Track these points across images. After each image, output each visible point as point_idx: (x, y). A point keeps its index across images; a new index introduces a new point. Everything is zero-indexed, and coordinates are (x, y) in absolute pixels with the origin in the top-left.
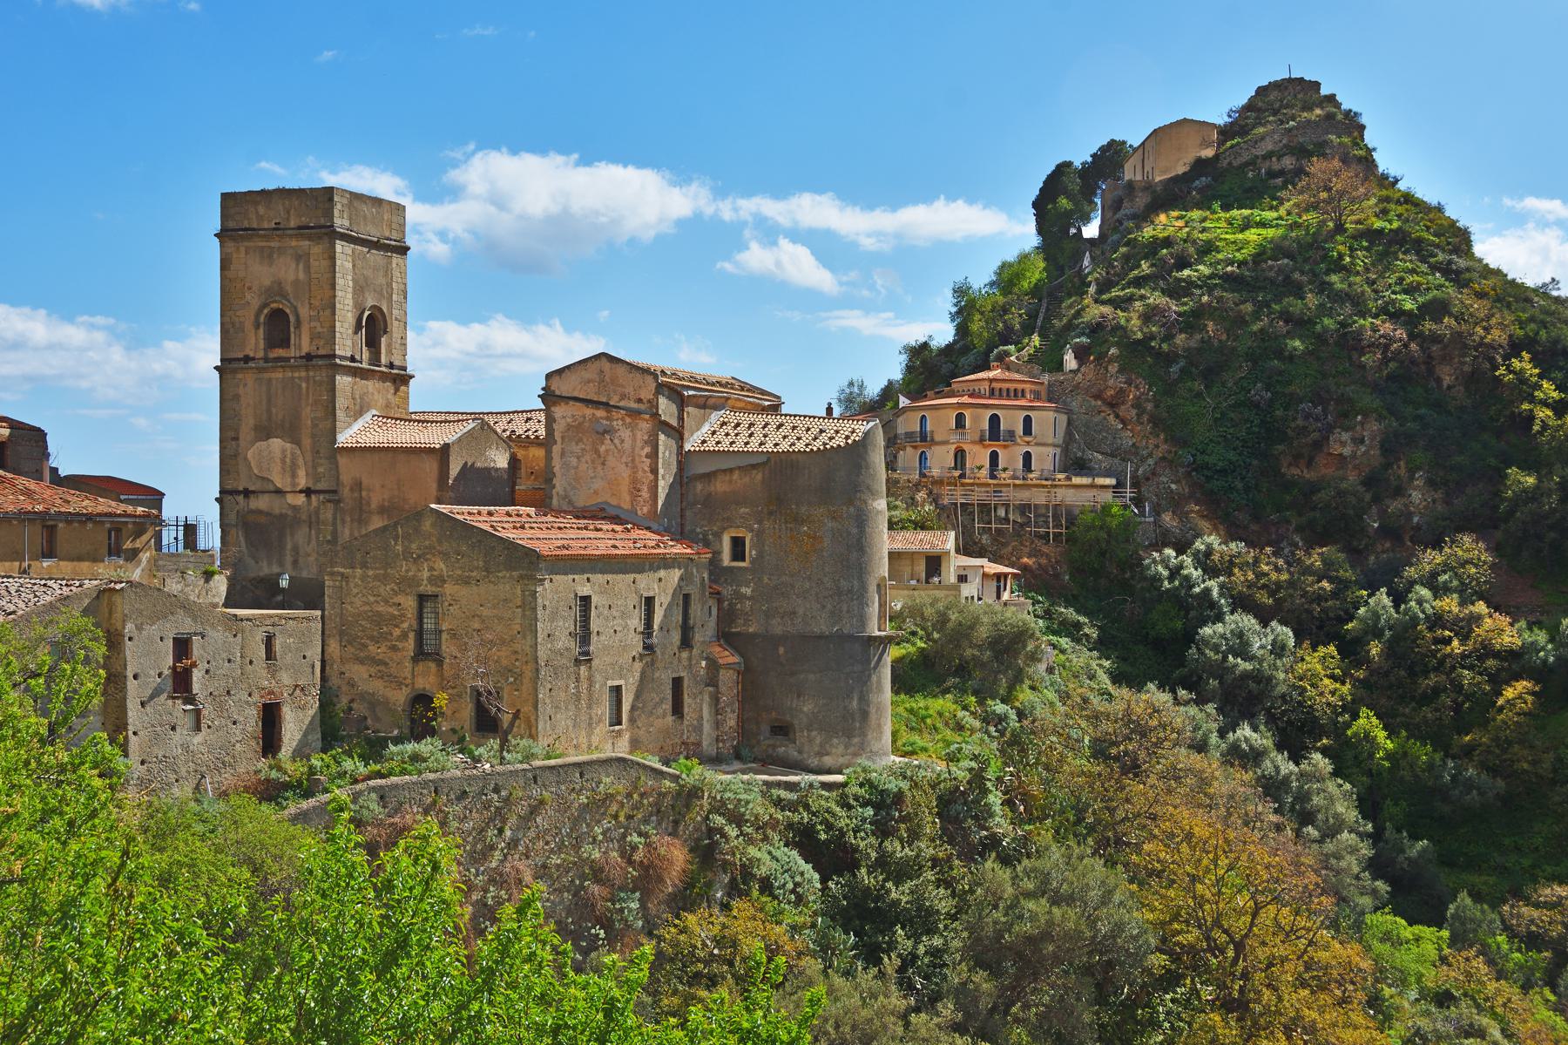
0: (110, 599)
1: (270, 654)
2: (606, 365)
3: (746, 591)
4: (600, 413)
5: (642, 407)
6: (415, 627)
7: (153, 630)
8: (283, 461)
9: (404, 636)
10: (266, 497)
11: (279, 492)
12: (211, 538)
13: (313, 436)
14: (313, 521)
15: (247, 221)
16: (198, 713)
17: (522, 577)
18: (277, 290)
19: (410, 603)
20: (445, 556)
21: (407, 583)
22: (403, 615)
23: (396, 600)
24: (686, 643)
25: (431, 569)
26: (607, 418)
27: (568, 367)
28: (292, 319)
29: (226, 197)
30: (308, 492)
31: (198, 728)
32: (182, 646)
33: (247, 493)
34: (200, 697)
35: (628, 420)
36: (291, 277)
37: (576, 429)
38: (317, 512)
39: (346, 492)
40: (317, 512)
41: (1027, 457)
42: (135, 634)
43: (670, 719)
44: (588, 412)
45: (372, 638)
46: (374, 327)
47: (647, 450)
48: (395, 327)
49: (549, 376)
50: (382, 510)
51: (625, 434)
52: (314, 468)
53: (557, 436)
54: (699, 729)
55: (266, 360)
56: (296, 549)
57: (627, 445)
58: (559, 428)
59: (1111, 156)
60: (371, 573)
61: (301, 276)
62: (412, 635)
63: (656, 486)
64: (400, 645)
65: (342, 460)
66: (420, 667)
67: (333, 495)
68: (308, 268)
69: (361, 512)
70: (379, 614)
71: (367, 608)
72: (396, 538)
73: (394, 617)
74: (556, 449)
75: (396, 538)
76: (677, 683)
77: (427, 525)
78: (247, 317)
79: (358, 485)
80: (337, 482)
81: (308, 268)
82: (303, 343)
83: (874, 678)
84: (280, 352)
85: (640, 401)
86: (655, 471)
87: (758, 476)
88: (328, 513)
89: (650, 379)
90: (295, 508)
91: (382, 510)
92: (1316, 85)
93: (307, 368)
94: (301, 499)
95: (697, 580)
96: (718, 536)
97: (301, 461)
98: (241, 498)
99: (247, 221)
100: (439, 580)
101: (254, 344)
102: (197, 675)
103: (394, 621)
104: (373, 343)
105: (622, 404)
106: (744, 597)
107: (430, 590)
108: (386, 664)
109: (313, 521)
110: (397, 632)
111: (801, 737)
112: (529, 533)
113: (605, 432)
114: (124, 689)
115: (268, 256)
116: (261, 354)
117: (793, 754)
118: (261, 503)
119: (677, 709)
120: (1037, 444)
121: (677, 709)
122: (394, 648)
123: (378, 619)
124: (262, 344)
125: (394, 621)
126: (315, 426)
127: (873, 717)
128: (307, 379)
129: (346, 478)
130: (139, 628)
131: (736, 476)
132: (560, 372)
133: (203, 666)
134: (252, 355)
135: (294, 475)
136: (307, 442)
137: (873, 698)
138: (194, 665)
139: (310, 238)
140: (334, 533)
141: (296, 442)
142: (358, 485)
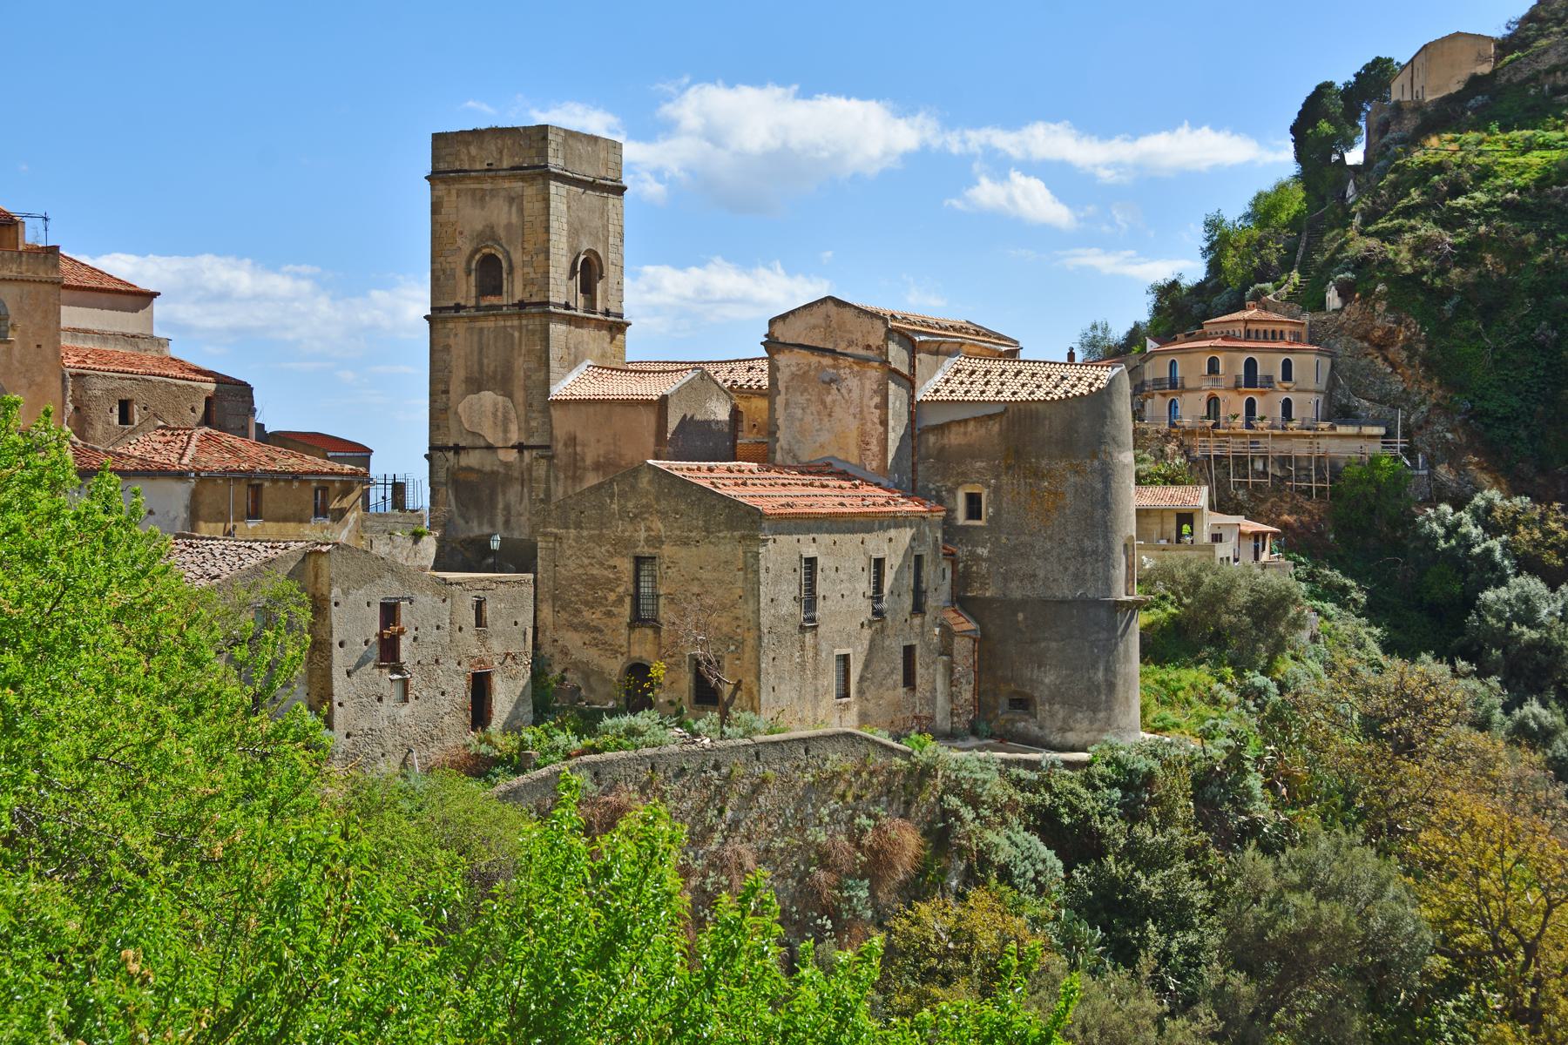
0: (315, 562)
1: (480, 621)
2: (831, 309)
3: (983, 551)
4: (827, 361)
6: (632, 591)
7: (360, 595)
8: (495, 415)
9: (620, 600)
11: (490, 448)
12: (420, 497)
13: (526, 388)
14: (526, 479)
15: (459, 162)
16: (405, 682)
17: (743, 537)
18: (489, 235)
23: (611, 562)
24: (918, 608)
25: (649, 529)
26: (834, 367)
27: (792, 312)
28: (505, 265)
29: (438, 138)
30: (520, 448)
32: (389, 612)
33: (457, 449)
34: (408, 666)
35: (856, 368)
36: (503, 220)
37: (801, 378)
41: (1287, 405)
42: (341, 599)
43: (901, 690)
44: (814, 359)
45: (586, 603)
46: (589, 272)
47: (877, 400)
48: (610, 271)
49: (772, 322)
50: (597, 467)
51: (853, 383)
54: (932, 702)
55: (478, 308)
56: (507, 508)
57: (855, 395)
58: (783, 377)
61: (515, 219)
62: (628, 600)
63: (886, 439)
65: (556, 414)
68: (521, 210)
71: (580, 571)
72: (612, 497)
73: (609, 581)
74: (780, 400)
75: (612, 497)
76: (909, 652)
77: (644, 481)
78: (458, 263)
79: (572, 440)
80: (551, 437)
81: (521, 210)
82: (516, 290)
84: (493, 300)
85: (868, 347)
86: (884, 423)
87: (995, 428)
88: (541, 470)
89: (879, 323)
90: (506, 465)
91: (597, 467)
93: (520, 316)
94: (512, 456)
95: (930, 540)
96: (952, 492)
97: (513, 415)
99: (459, 162)
101: (465, 290)
102: (405, 643)
103: (609, 585)
104: (588, 289)
105: (849, 351)
107: (646, 551)
108: (600, 631)
109: (526, 479)
110: (612, 597)
111: (1043, 710)
112: (750, 490)
113: (832, 381)
114: (329, 657)
115: (481, 198)
116: (472, 302)
117: (1034, 729)
118: (471, 459)
119: (909, 680)
120: (1298, 391)
121: (909, 680)
122: (609, 614)
125: (609, 585)
126: (528, 377)
127: (1120, 689)
128: (520, 328)
129: (560, 432)
130: (346, 593)
131: (971, 426)
132: (783, 317)
133: (411, 633)
134: (463, 303)
135: (506, 431)
136: (519, 395)
137: (1120, 668)
138: (402, 632)
139: (523, 179)
140: (548, 491)
141: (509, 395)
142: (572, 440)
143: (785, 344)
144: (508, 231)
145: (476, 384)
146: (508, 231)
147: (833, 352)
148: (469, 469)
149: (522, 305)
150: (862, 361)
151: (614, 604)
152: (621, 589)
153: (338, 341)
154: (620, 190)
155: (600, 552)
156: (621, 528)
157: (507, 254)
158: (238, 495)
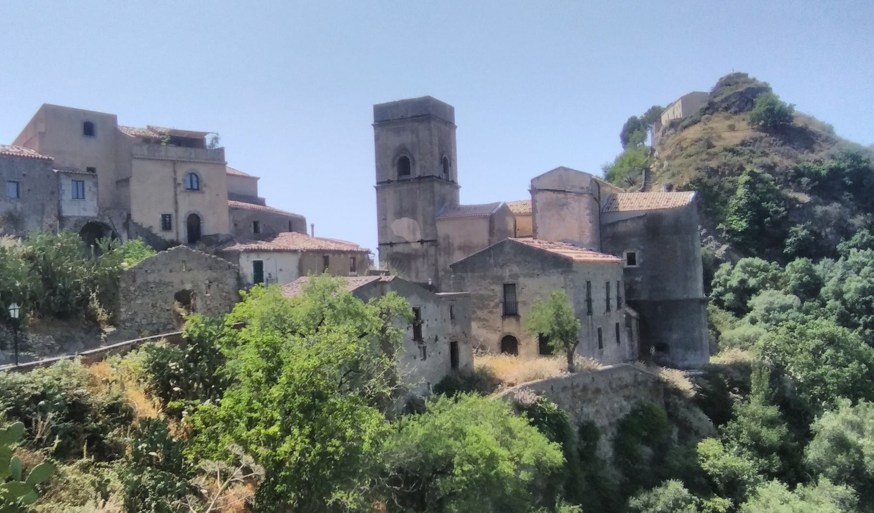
0: (382, 287)
4: (561, 196)
5: (582, 191)
8: (409, 228)
9: (497, 306)
10: (401, 245)
11: (407, 243)
14: (425, 255)
15: (389, 119)
16: (424, 348)
18: (403, 149)
19: (499, 289)
20: (518, 264)
21: (496, 279)
22: (496, 295)
23: (492, 288)
25: (510, 270)
30: (422, 242)
31: (425, 358)
33: (391, 244)
34: (425, 340)
35: (576, 198)
37: (548, 205)
38: (427, 251)
39: (441, 240)
40: (427, 251)
45: (479, 308)
49: (532, 181)
50: (461, 248)
52: (424, 230)
53: (538, 209)
55: (398, 181)
56: (417, 269)
58: (539, 205)
59: (655, 114)
60: (476, 274)
62: (501, 305)
64: (494, 310)
66: (507, 321)
67: (434, 242)
69: (449, 250)
70: (482, 295)
72: (490, 256)
73: (491, 296)
74: (538, 216)
75: (490, 256)
77: (507, 249)
83: (636, 345)
85: (582, 188)
87: (641, 223)
88: (432, 251)
90: (416, 250)
91: (461, 248)
92: (746, 75)
98: (389, 247)
99: (389, 119)
100: (516, 276)
101: (392, 174)
103: (491, 298)
106: (637, 282)
107: (511, 281)
109: (425, 255)
110: (492, 304)
116: (396, 179)
117: (668, 359)
118: (398, 249)
123: (481, 298)
124: (396, 174)
125: (491, 298)
131: (629, 223)
132: (538, 178)
133: (426, 323)
135: (414, 234)
136: (420, 218)
138: (422, 322)
140: (436, 260)
141: (415, 218)
143: (540, 190)
144: (414, 147)
145: (400, 214)
146: (414, 147)
147: (564, 191)
148: (397, 253)
149: (420, 179)
150: (580, 194)
151: (494, 307)
152: (497, 300)
153: (336, 200)
154: (290, 231)
155: (484, 283)
156: (497, 271)
157: (412, 155)
158: (319, 259)
